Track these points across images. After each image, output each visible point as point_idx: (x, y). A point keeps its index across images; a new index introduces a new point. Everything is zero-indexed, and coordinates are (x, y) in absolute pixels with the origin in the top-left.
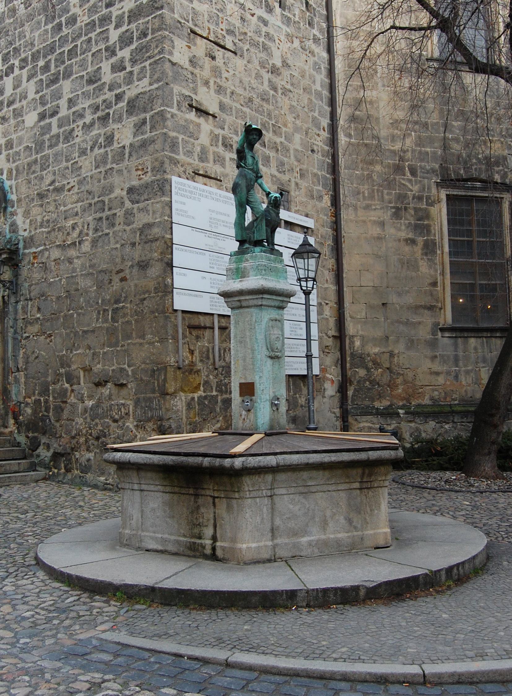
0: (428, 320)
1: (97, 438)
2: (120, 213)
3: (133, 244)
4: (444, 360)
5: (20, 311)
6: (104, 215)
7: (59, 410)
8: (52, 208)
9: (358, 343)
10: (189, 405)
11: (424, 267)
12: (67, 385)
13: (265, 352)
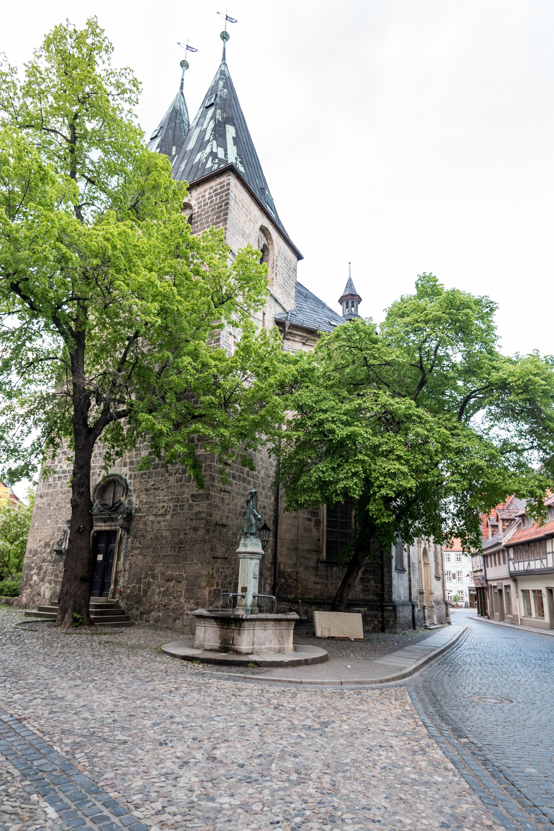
0: (315, 557)
1: (165, 606)
2: (187, 505)
3: (192, 520)
4: (321, 577)
5: (130, 543)
6: (178, 504)
7: (146, 592)
8: (152, 497)
9: (282, 566)
10: (210, 592)
11: (314, 532)
12: (151, 580)
13: (252, 576)
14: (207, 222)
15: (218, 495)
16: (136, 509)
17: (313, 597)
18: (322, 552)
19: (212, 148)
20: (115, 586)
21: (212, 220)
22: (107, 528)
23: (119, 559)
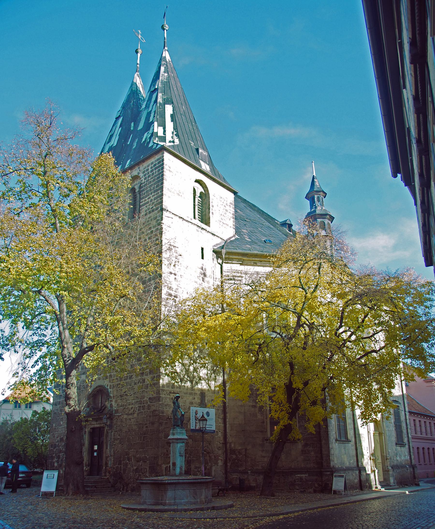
3: (150, 416)
5: (113, 435)
8: (125, 401)
9: (233, 445)
14: (151, 190)
15: (168, 396)
16: (115, 410)
17: (260, 468)
18: (266, 431)
19: (153, 129)
20: (106, 468)
21: (154, 188)
22: (98, 426)
23: (107, 448)
